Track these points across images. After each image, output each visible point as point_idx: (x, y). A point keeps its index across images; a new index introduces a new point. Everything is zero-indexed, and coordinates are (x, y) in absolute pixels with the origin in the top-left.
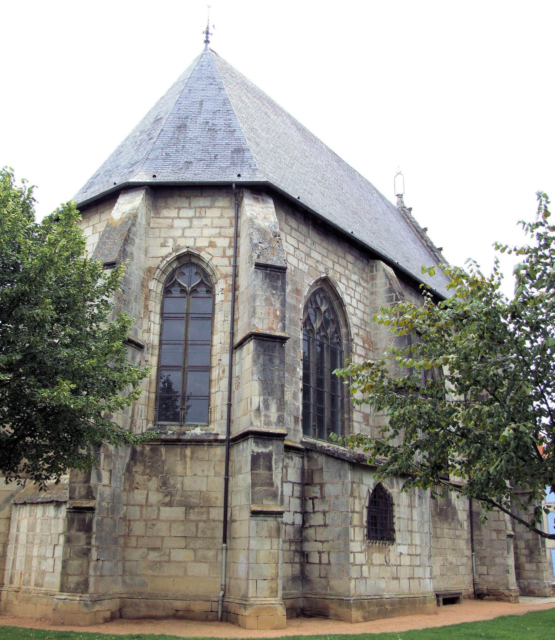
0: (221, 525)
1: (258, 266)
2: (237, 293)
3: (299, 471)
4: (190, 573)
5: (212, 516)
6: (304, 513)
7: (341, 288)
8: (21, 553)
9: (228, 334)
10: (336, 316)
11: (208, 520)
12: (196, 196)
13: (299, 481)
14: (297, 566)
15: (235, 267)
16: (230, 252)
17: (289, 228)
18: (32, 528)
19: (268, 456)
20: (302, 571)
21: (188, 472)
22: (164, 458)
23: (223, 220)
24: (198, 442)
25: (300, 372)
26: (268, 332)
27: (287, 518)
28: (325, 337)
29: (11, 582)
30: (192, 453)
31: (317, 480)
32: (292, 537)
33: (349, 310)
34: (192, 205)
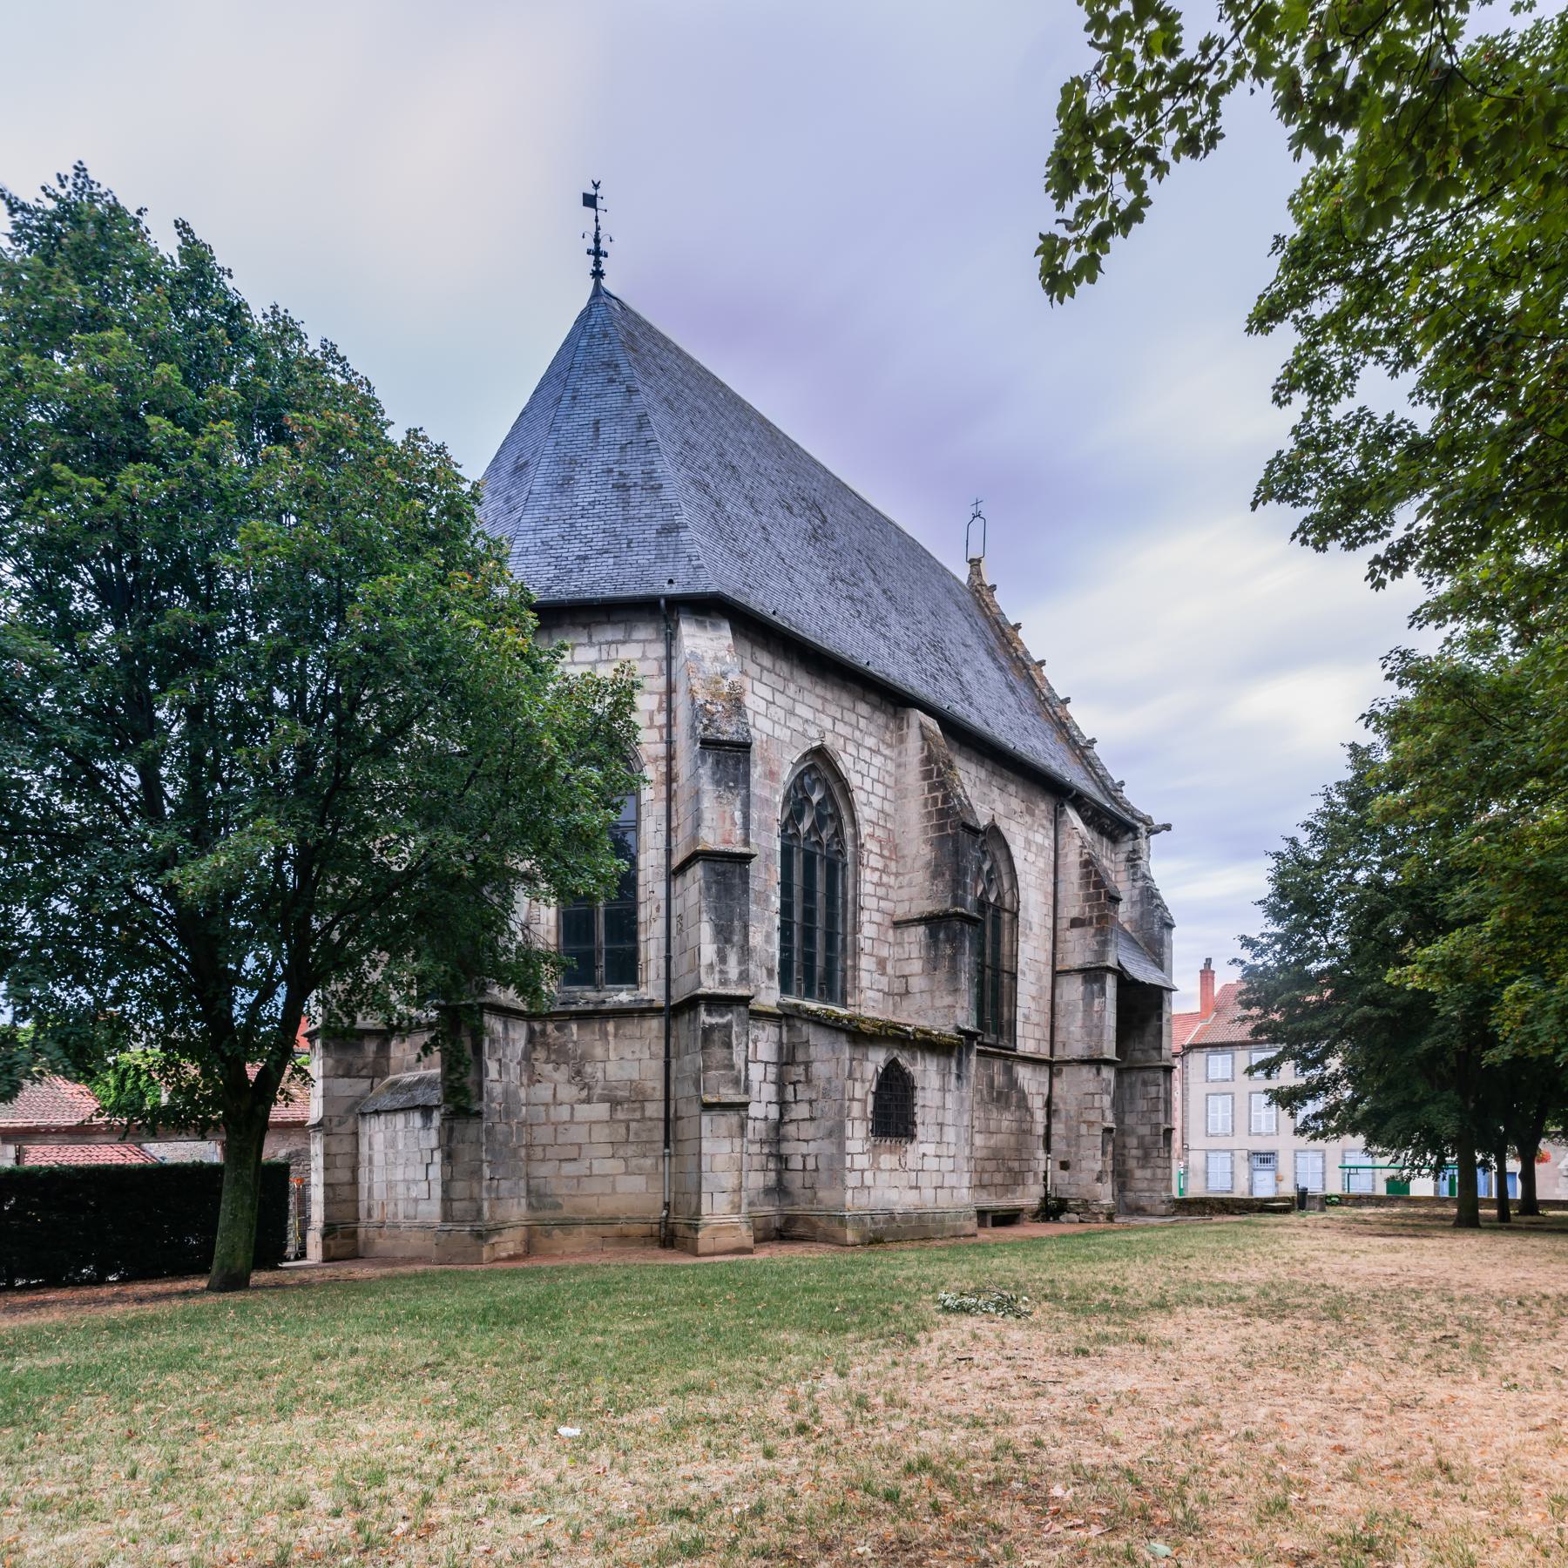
0: (661, 1125)
1: (706, 744)
2: (674, 786)
3: (774, 1047)
4: (619, 1189)
5: (648, 1114)
6: (782, 1104)
7: (845, 763)
8: (379, 1177)
9: (662, 852)
10: (837, 809)
11: (643, 1119)
12: (599, 623)
13: (774, 1059)
14: (773, 1175)
15: (670, 743)
16: (661, 719)
17: (758, 669)
18: (391, 1144)
19: (728, 1026)
20: (779, 1180)
21: (612, 1055)
22: (575, 1038)
23: (648, 663)
24: (623, 1014)
25: (776, 902)
26: (722, 848)
27: (755, 1110)
28: (818, 843)
29: (370, 1216)
30: (617, 1029)
31: (800, 1057)
32: (764, 1136)
33: (859, 797)
34: (594, 640)
